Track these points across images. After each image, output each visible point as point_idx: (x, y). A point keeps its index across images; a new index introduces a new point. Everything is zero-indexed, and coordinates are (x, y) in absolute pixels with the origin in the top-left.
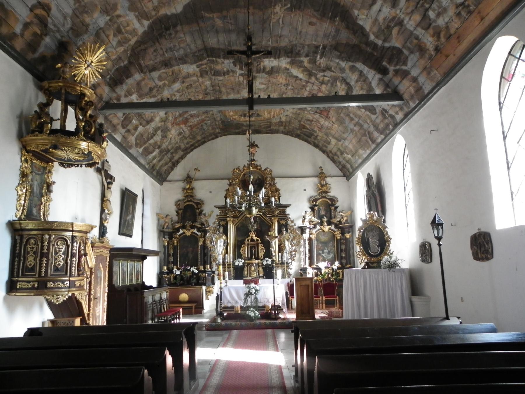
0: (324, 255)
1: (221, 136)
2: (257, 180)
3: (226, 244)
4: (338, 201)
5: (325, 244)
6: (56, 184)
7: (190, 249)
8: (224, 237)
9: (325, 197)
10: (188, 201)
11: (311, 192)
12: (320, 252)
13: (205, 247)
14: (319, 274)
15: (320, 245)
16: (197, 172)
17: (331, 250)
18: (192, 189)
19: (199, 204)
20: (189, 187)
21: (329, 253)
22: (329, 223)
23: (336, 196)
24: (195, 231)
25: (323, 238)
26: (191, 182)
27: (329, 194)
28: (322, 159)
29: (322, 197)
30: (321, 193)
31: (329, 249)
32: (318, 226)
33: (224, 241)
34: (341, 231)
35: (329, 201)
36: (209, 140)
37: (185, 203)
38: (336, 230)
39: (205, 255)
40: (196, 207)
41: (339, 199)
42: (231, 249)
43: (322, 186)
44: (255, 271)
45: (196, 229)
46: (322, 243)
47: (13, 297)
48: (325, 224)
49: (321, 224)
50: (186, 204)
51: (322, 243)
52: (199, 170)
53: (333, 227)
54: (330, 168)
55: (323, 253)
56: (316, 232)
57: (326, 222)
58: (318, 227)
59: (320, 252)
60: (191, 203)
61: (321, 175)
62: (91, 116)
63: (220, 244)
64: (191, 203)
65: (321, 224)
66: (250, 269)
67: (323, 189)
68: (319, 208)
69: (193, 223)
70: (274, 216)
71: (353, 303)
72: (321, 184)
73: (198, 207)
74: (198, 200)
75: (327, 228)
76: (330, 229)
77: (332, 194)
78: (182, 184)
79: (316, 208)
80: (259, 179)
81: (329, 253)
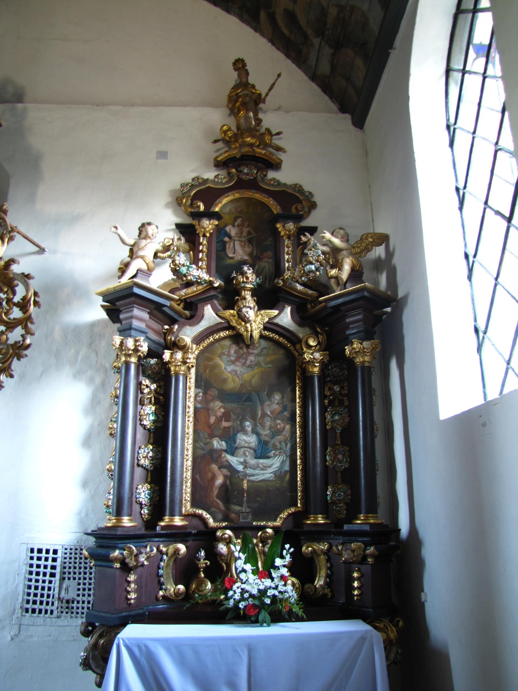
0: (234, 461)
4: (313, 206)
5: (243, 402)
6: (26, 359)
9: (253, 185)
11: (194, 166)
12: (218, 444)
14: (203, 563)
15: (218, 407)
17: (276, 432)
22: (266, 298)
23: (307, 188)
25: (234, 371)
27: (271, 174)
29: (240, 185)
31: (265, 432)
32: (208, 310)
34: (330, 336)
35: (271, 202)
38: (301, 332)
41: (317, 198)
46: (225, 396)
47: (236, 454)
48: (250, 301)
51: (225, 396)
53: (286, 318)
54: (267, 63)
55: (232, 451)
56: (198, 340)
57: (255, 293)
58: (210, 315)
59: (218, 444)
62: (271, 412)
65: (230, 296)
67: (246, 157)
68: (220, 231)
71: (294, 291)
75: (255, 319)
76: (270, 326)
77: (285, 176)
81: (262, 451)
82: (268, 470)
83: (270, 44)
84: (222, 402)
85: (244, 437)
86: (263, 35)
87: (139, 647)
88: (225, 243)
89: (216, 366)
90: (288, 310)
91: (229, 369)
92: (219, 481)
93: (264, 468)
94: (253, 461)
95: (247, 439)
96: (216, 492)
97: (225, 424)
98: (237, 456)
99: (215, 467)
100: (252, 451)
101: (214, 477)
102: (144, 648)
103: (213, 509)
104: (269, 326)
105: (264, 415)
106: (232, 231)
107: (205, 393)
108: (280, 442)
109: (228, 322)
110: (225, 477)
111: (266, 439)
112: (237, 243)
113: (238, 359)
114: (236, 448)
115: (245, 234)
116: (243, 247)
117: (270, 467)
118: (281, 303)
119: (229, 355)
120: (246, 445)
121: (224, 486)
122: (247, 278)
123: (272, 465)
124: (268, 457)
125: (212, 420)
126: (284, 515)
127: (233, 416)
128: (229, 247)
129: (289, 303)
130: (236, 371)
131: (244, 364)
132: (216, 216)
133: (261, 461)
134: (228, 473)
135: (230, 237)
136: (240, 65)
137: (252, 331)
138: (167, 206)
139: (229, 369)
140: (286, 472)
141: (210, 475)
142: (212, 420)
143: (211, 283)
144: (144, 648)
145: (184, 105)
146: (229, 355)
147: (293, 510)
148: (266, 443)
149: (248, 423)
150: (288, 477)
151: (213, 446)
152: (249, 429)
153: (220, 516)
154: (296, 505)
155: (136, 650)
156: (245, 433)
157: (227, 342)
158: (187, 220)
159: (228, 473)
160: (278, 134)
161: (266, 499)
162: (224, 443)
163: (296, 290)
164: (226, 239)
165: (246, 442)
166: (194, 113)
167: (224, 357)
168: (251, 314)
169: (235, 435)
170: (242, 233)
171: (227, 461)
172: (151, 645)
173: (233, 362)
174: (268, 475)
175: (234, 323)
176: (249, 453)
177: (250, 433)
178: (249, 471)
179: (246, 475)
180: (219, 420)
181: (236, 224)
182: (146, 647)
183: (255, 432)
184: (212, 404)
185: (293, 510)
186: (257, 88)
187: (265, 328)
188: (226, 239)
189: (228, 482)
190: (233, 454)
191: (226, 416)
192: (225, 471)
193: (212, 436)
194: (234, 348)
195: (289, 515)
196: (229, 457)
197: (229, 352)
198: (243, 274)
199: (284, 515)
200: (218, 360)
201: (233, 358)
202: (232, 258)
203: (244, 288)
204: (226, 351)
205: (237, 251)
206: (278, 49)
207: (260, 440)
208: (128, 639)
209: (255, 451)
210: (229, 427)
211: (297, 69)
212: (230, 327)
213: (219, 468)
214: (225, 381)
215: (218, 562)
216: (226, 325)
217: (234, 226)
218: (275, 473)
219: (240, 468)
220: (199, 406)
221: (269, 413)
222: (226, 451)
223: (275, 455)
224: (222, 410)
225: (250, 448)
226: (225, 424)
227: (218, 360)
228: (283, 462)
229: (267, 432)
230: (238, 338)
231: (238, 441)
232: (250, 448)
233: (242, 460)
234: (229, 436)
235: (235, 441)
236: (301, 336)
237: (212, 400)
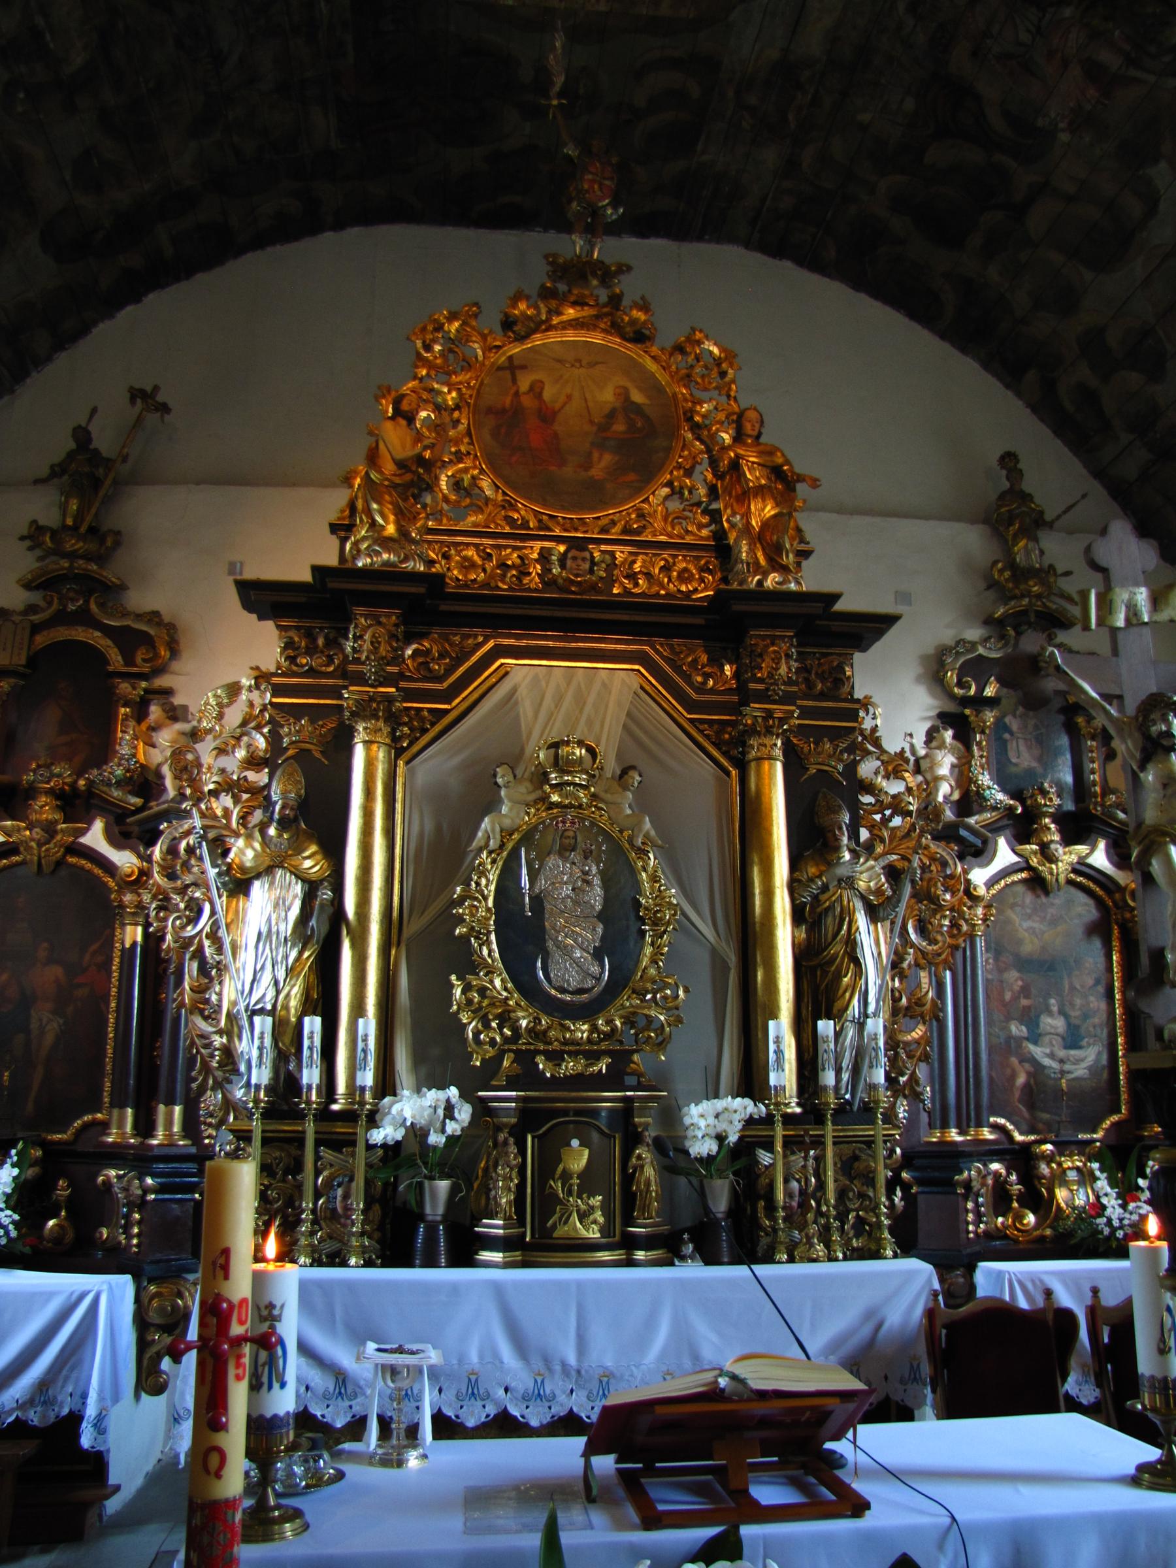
0: (1037, 1051)
1: (339, 225)
2: (611, 415)
3: (323, 932)
5: (1045, 968)
7: (47, 976)
8: (311, 863)
10: (62, 618)
12: (1017, 1029)
13: (157, 965)
15: (1013, 976)
16: (152, 419)
18: (104, 540)
19: (147, 640)
20: (79, 517)
21: (1072, 1040)
22: (1077, 829)
24: (96, 837)
26: (97, 484)
28: (995, 417)
30: (1019, 621)
33: (311, 889)
36: (260, 241)
37: (36, 629)
39: (155, 1017)
40: (116, 660)
42: (360, 973)
43: (1021, 574)
44: (589, 1182)
45: (98, 826)
46: (1024, 964)
49: (1023, 828)
50: (42, 640)
52: (164, 408)
53: (1100, 858)
54: (1054, 473)
55: (1035, 1038)
56: (990, 884)
58: (1004, 855)
59: (1017, 1029)
60: (81, 634)
61: (1011, 514)
63: (268, 911)
64: (81, 634)
66: (548, 1162)
68: (999, 722)
69: (79, 774)
70: (763, 697)
72: (1012, 565)
73: (129, 660)
74: (139, 617)
78: (44, 507)
79: (990, 717)
80: (629, 407)
81: (1072, 1040)
82: (1086, 1061)
83: (1028, 410)
84: (1019, 971)
85: (1049, 1020)
86: (1019, 394)
87: (1033, 1281)
88: (1005, 742)
89: (1008, 921)
90: (1102, 845)
91: (1026, 925)
92: (1021, 1080)
93: (1078, 1061)
94: (1062, 1053)
95: (1053, 1023)
96: (1017, 1094)
97: (1024, 1002)
98: (1042, 1046)
99: (1014, 1060)
100: (1059, 1039)
101: (1013, 1076)
102: (1038, 1283)
103: (1016, 1118)
104: (1078, 867)
105: (1073, 988)
106: (1013, 723)
107: (996, 959)
108: (1094, 1027)
109: (1027, 862)
110: (1029, 1074)
111: (1077, 1022)
112: (1021, 742)
113: (1035, 910)
114: (1040, 1035)
115: (1030, 728)
116: (1029, 748)
117: (1083, 1060)
118: (1093, 836)
119: (1023, 906)
120: (1053, 1031)
121: (1027, 1085)
122: (1051, 800)
123: (1086, 1058)
124: (1080, 1048)
125: (1008, 996)
126: (1107, 1124)
127: (1033, 991)
128: (1012, 747)
129: (1104, 835)
130: (1033, 929)
131: (1043, 919)
132: (992, 702)
133: (1072, 1052)
134: (1032, 1069)
135: (1012, 733)
136: (1009, 460)
137: (1058, 874)
138: (918, 679)
139: (1026, 925)
140: (1103, 1067)
141: (1008, 1071)
142: (1008, 996)
143: (1011, 809)
144: (1038, 1283)
145: (927, 517)
146: (1023, 906)
147: (1115, 1118)
148: (1077, 1027)
149: (1053, 1001)
150: (1105, 1075)
151: (1010, 1031)
152: (1055, 1009)
153: (1024, 1127)
154: (1119, 1112)
155: (1030, 1286)
156: (1050, 1013)
157: (1020, 889)
158: (951, 707)
159: (1032, 1069)
160: (1067, 574)
161: (1090, 1103)
162: (1024, 1028)
163: (1116, 819)
164: (1007, 736)
165: (1052, 1027)
166: (944, 530)
167: (1018, 909)
168: (1059, 850)
169: (1038, 1017)
170: (1026, 727)
171: (1030, 1053)
172: (1046, 1279)
173: (1029, 917)
174: (1080, 1071)
175: (1034, 862)
176: (1057, 1041)
177: (1056, 1014)
178: (1067, 1067)
179: (1063, 1072)
180: (1015, 998)
181: (1018, 713)
182: (1041, 1281)
183: (1062, 1012)
184: (1006, 975)
185: (1115, 1118)
186: (1036, 500)
187: (1074, 871)
188: (1007, 736)
189: (1032, 1082)
190: (1036, 1043)
191: (1025, 991)
192: (1027, 1066)
193: (1009, 1018)
194: (1029, 898)
195: (1113, 1124)
196: (1032, 1047)
197: (1023, 902)
198: (1044, 793)
199: (1107, 1124)
200: (1010, 914)
201: (1029, 911)
202: (1016, 765)
203: (1045, 815)
204: (1019, 900)
205: (1022, 757)
206: (1042, 420)
207: (1069, 1025)
208: (1021, 1273)
209: (1063, 1038)
210: (1029, 1007)
211: (1070, 454)
212: (1029, 868)
213: (1021, 1062)
214: (1020, 942)
215: (1034, 1186)
216: (1024, 865)
217: (1015, 716)
218: (1089, 1068)
219: (1047, 1062)
220: (990, 977)
221: (1078, 987)
222: (1027, 1039)
223: (1089, 1045)
224: (1020, 983)
225: (1057, 1035)
226: (1024, 1002)
227: (1010, 914)
228: (1099, 1053)
229: (1078, 1013)
230: (1037, 883)
231: (1042, 1025)
232: (1057, 1035)
233: (1048, 1051)
234: (1030, 1018)
235: (1038, 1026)
236: (1122, 882)
237: (1006, 970)
